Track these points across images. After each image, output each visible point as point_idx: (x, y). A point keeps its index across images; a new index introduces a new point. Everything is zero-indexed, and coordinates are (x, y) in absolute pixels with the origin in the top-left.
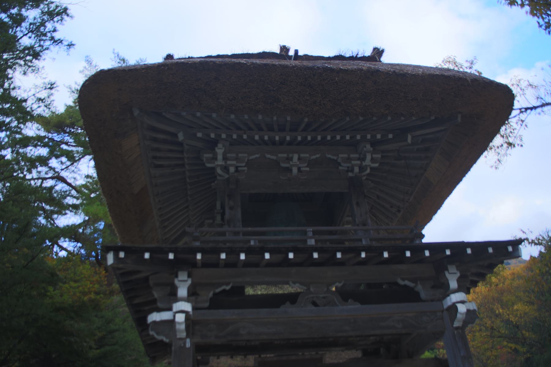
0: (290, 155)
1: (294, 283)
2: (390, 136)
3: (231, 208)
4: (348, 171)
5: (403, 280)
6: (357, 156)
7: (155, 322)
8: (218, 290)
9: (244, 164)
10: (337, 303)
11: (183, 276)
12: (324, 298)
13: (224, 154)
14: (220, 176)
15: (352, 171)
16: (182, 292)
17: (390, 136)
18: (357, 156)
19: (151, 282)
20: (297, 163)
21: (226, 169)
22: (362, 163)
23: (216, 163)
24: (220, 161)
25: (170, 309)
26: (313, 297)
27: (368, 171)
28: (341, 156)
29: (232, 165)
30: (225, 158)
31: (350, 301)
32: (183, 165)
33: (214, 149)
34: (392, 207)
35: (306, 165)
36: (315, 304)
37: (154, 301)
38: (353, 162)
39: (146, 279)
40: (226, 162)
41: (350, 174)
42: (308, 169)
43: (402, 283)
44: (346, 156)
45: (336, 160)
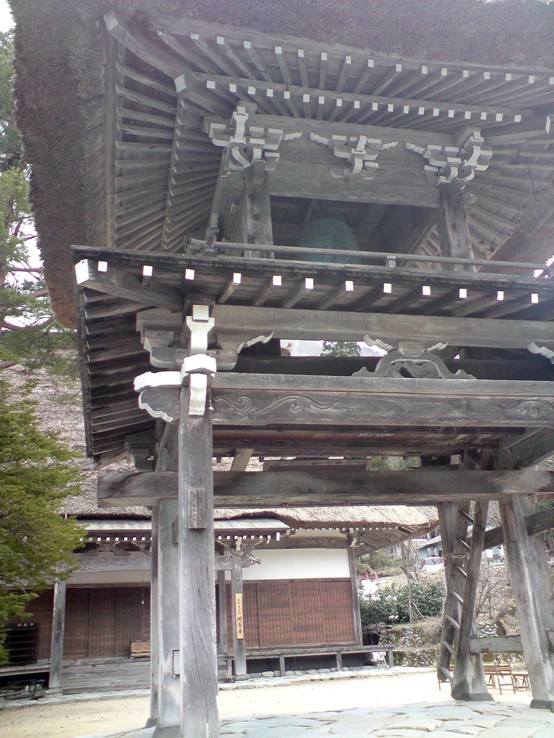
0: (353, 139)
1: (374, 338)
2: (518, 119)
3: (256, 217)
4: (438, 175)
5: (540, 345)
6: (456, 150)
7: (148, 389)
8: (250, 343)
9: (275, 147)
10: (440, 374)
11: (200, 312)
12: (420, 364)
13: (247, 125)
14: (236, 162)
15: (447, 173)
16: (199, 337)
17: (518, 119)
18: (456, 150)
19: (139, 324)
20: (365, 150)
21: (247, 152)
22: (463, 164)
23: (232, 140)
24: (239, 139)
25: (177, 368)
26: (403, 363)
27: (472, 176)
28: (431, 147)
29: (258, 146)
30: (248, 135)
31: (459, 372)
32: (169, 142)
33: (230, 116)
34: (482, 243)
35: (374, 157)
36: (405, 373)
37: (146, 355)
38: (450, 160)
39: (131, 318)
40: (248, 140)
41: (443, 179)
42: (376, 165)
43: (535, 350)
44: (439, 148)
45: (421, 155)
